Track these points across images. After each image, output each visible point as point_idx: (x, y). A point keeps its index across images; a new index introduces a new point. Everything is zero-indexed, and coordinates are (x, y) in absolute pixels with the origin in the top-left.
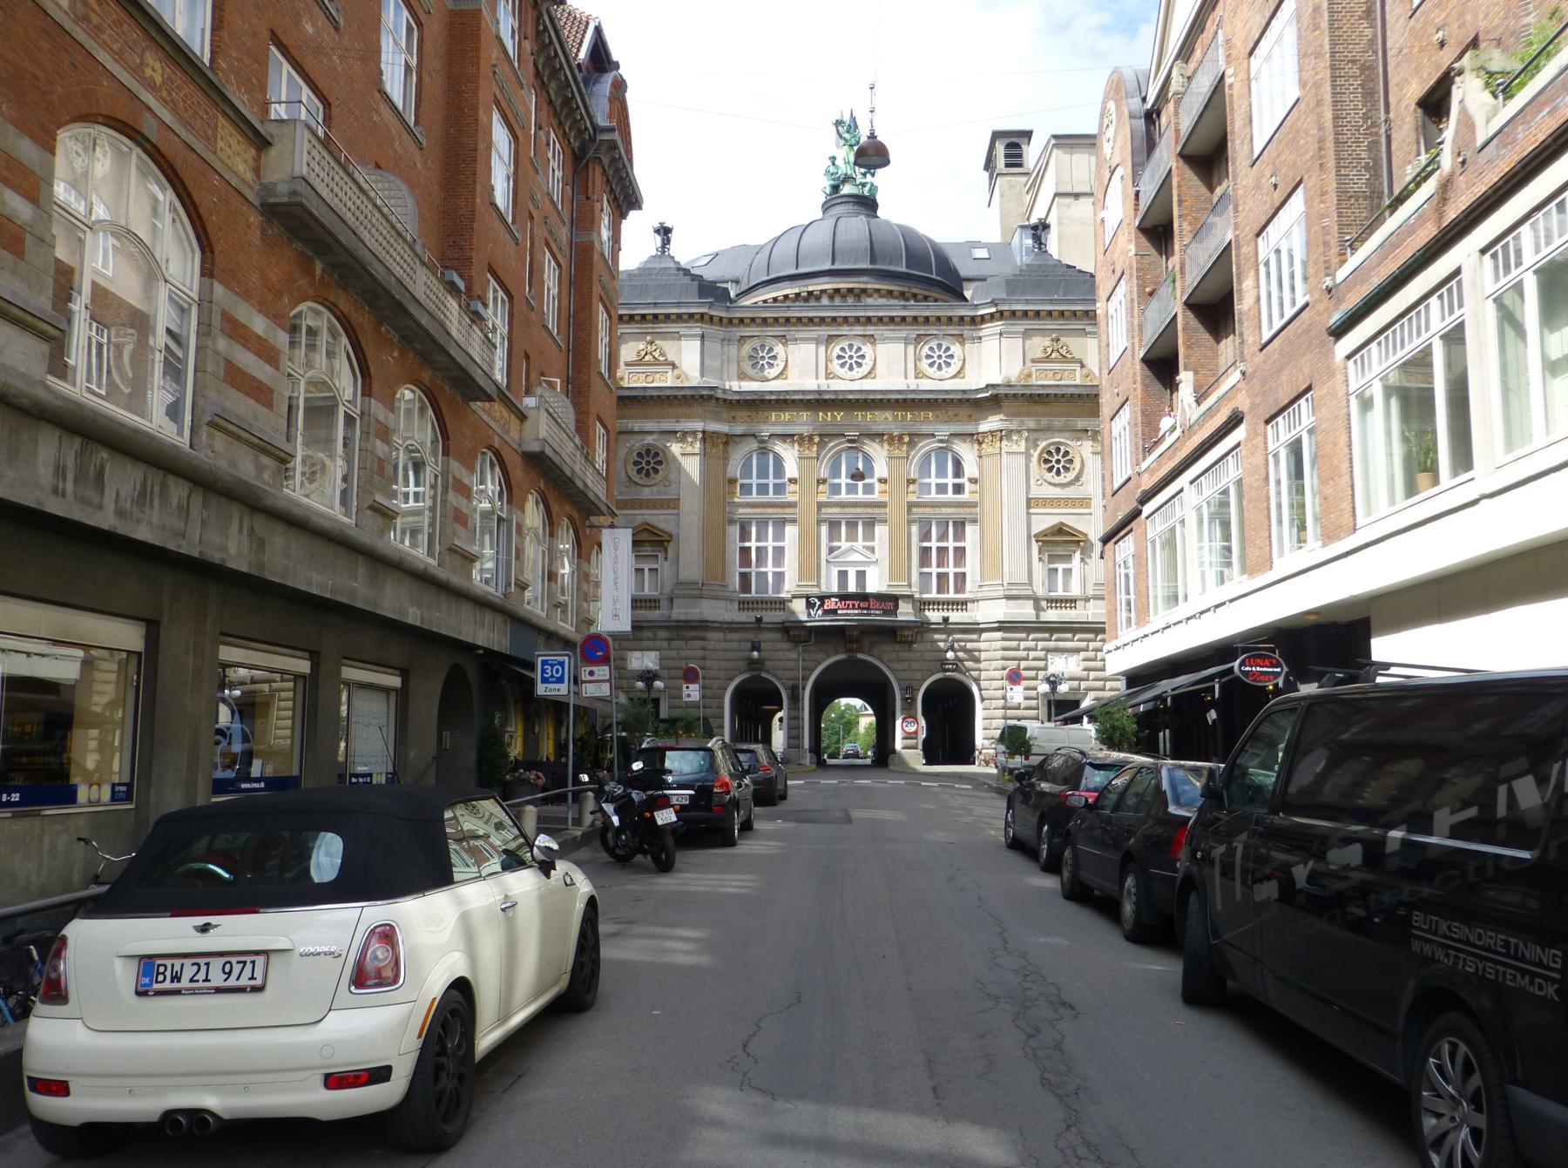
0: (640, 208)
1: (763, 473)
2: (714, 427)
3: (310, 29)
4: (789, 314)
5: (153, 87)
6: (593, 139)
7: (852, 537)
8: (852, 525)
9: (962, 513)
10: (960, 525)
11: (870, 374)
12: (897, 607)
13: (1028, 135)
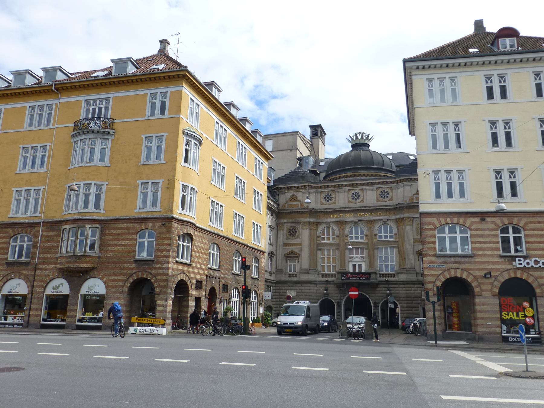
0: (482, 20)
1: (329, 234)
2: (312, 220)
7: (357, 253)
8: (357, 249)
11: (362, 201)
12: (370, 276)
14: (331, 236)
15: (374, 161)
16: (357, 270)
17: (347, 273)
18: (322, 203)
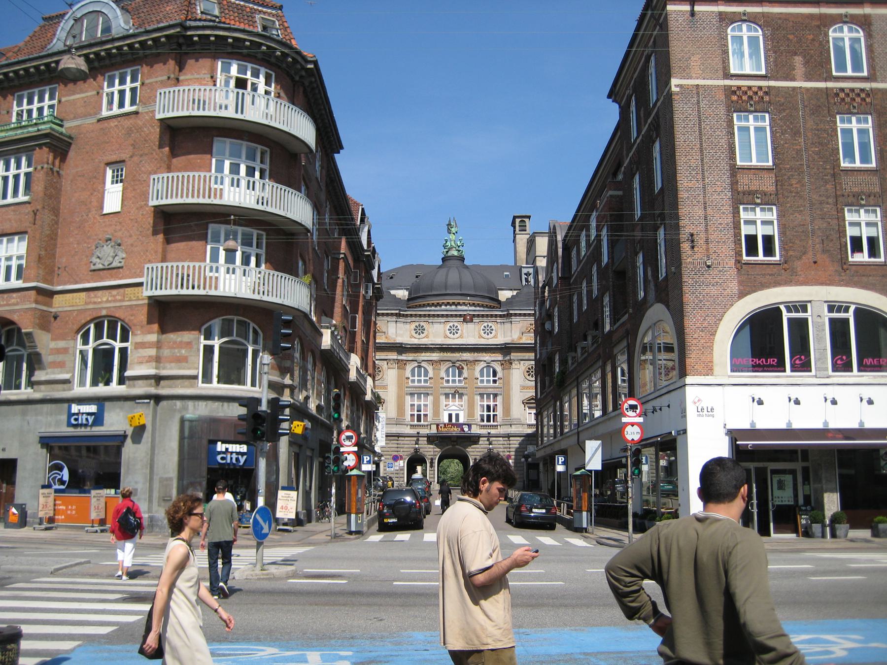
1: (419, 375)
10: (495, 395)
11: (495, 337)
13: (529, 217)
14: (423, 378)
16: (454, 421)
18: (446, 337)
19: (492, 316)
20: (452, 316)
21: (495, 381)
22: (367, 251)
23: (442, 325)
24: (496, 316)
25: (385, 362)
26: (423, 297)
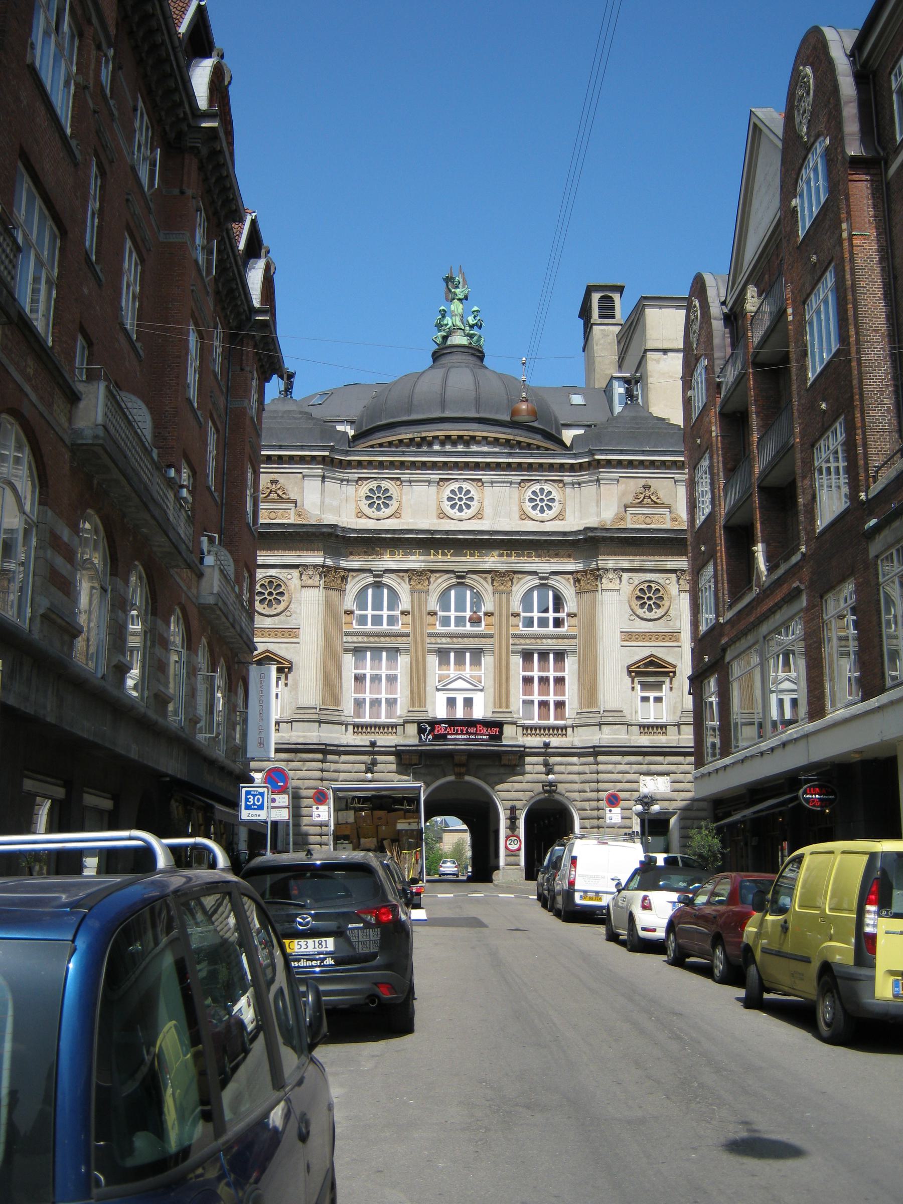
1: (377, 606)
3: (86, 291)
4: (390, 439)
5: (28, 380)
6: (249, 319)
9: (560, 645)
10: (560, 656)
11: (560, 516)
12: (501, 733)
13: (620, 289)
14: (385, 613)
15: (415, 402)
17: (434, 723)
18: (442, 515)
19: (551, 467)
20: (456, 466)
21: (558, 623)
22: (206, 115)
23: (433, 489)
24: (562, 467)
25: (295, 573)
26: (386, 436)
